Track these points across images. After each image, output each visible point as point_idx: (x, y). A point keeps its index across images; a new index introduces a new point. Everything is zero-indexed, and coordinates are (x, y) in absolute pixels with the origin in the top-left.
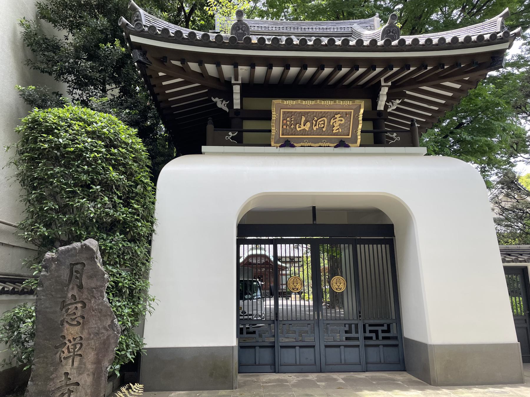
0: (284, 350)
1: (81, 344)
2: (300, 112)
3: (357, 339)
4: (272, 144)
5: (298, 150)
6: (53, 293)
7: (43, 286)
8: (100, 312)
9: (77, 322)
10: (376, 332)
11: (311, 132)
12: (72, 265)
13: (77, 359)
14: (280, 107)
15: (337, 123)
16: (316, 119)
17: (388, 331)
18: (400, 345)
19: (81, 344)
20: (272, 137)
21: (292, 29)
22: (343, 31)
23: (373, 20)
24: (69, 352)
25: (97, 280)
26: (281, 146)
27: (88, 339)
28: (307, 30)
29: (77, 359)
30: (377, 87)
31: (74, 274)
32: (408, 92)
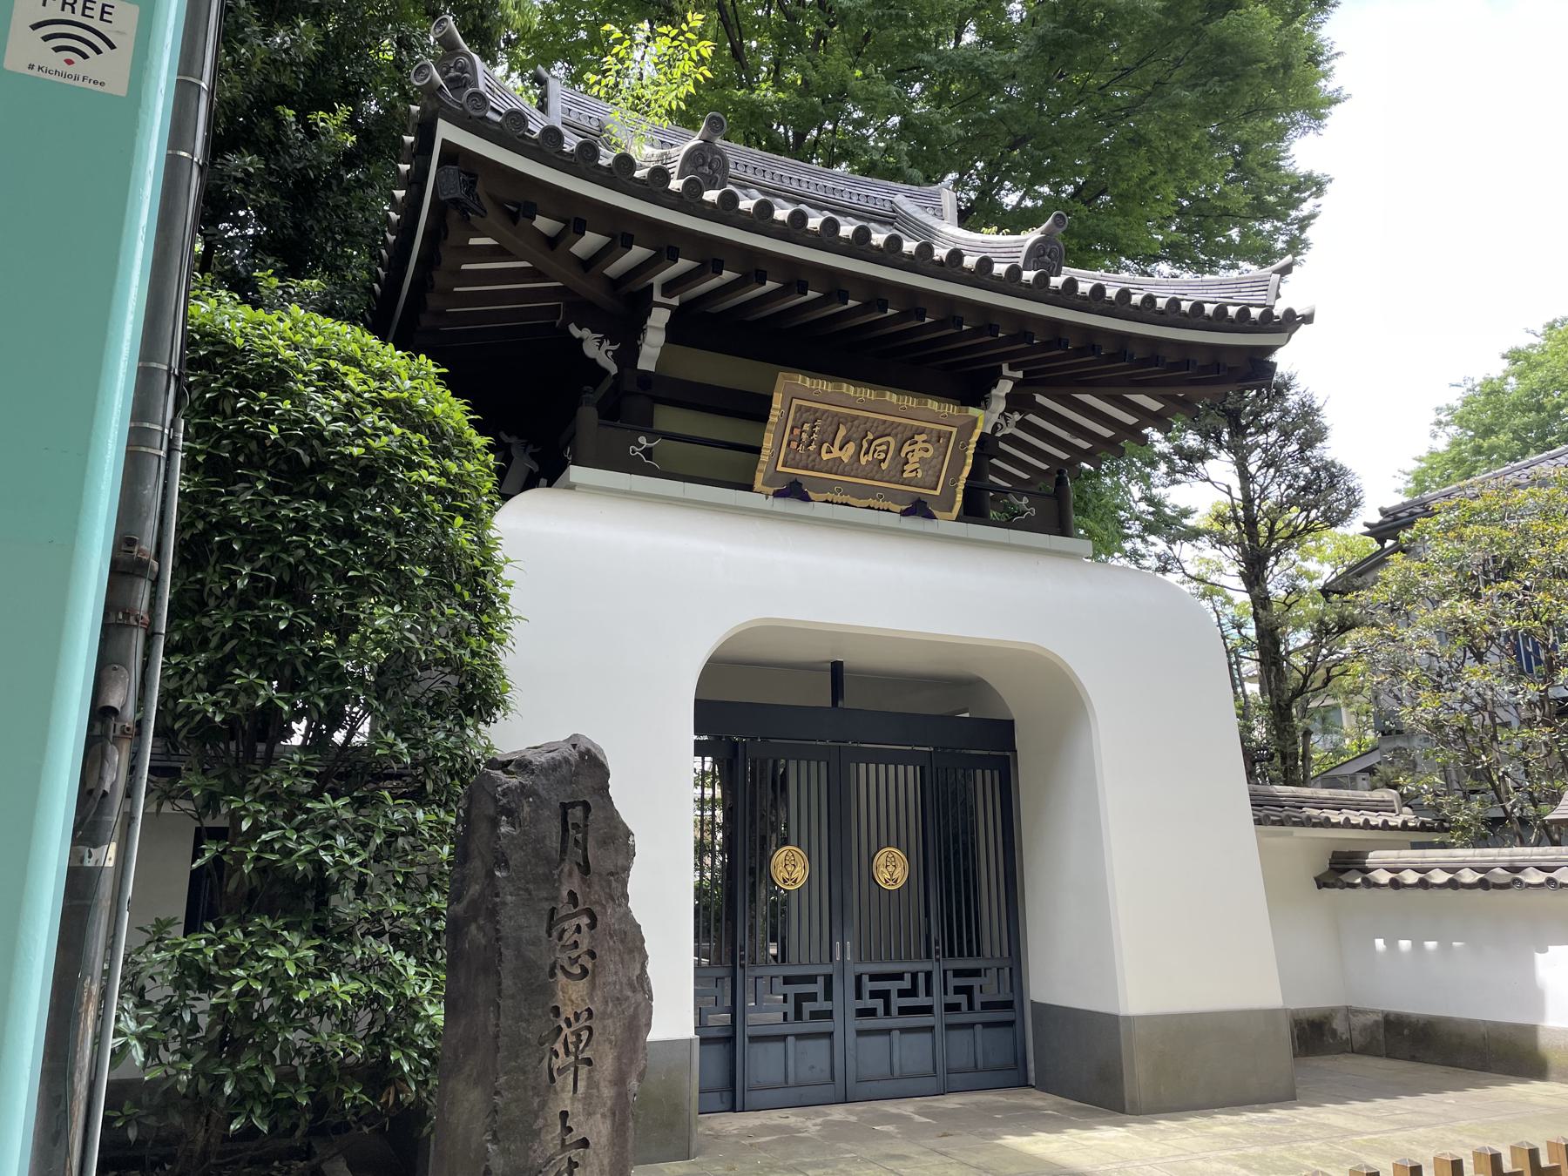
0: (758, 1048)
1: (590, 1029)
2: (837, 414)
3: (927, 1010)
4: (758, 485)
5: (818, 509)
6: (531, 887)
7: (507, 867)
8: (622, 941)
9: (582, 967)
10: (884, 995)
11: (853, 468)
12: (565, 807)
13: (584, 1071)
14: (795, 393)
15: (918, 453)
16: (870, 436)
17: (800, 999)
18: (1018, 1022)
19: (590, 1029)
20: (760, 466)
21: (750, 171)
22: (870, 206)
23: (938, 195)
24: (567, 1053)
25: (616, 850)
26: (777, 494)
27: (604, 1016)
28: (787, 181)
29: (584, 1071)
30: (641, 305)
31: (572, 832)
32: (1040, 399)
